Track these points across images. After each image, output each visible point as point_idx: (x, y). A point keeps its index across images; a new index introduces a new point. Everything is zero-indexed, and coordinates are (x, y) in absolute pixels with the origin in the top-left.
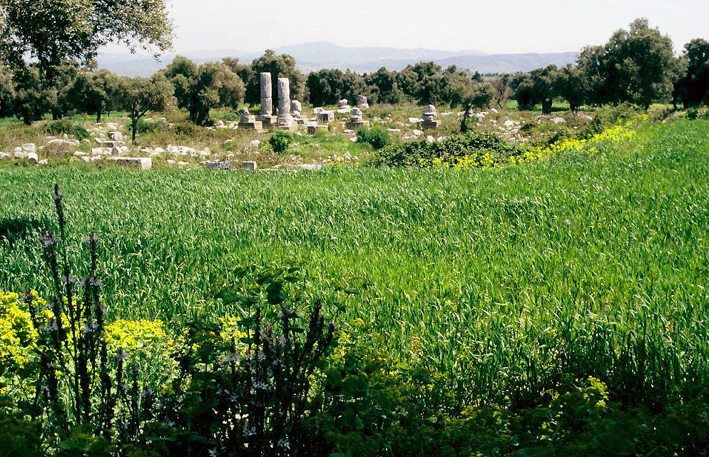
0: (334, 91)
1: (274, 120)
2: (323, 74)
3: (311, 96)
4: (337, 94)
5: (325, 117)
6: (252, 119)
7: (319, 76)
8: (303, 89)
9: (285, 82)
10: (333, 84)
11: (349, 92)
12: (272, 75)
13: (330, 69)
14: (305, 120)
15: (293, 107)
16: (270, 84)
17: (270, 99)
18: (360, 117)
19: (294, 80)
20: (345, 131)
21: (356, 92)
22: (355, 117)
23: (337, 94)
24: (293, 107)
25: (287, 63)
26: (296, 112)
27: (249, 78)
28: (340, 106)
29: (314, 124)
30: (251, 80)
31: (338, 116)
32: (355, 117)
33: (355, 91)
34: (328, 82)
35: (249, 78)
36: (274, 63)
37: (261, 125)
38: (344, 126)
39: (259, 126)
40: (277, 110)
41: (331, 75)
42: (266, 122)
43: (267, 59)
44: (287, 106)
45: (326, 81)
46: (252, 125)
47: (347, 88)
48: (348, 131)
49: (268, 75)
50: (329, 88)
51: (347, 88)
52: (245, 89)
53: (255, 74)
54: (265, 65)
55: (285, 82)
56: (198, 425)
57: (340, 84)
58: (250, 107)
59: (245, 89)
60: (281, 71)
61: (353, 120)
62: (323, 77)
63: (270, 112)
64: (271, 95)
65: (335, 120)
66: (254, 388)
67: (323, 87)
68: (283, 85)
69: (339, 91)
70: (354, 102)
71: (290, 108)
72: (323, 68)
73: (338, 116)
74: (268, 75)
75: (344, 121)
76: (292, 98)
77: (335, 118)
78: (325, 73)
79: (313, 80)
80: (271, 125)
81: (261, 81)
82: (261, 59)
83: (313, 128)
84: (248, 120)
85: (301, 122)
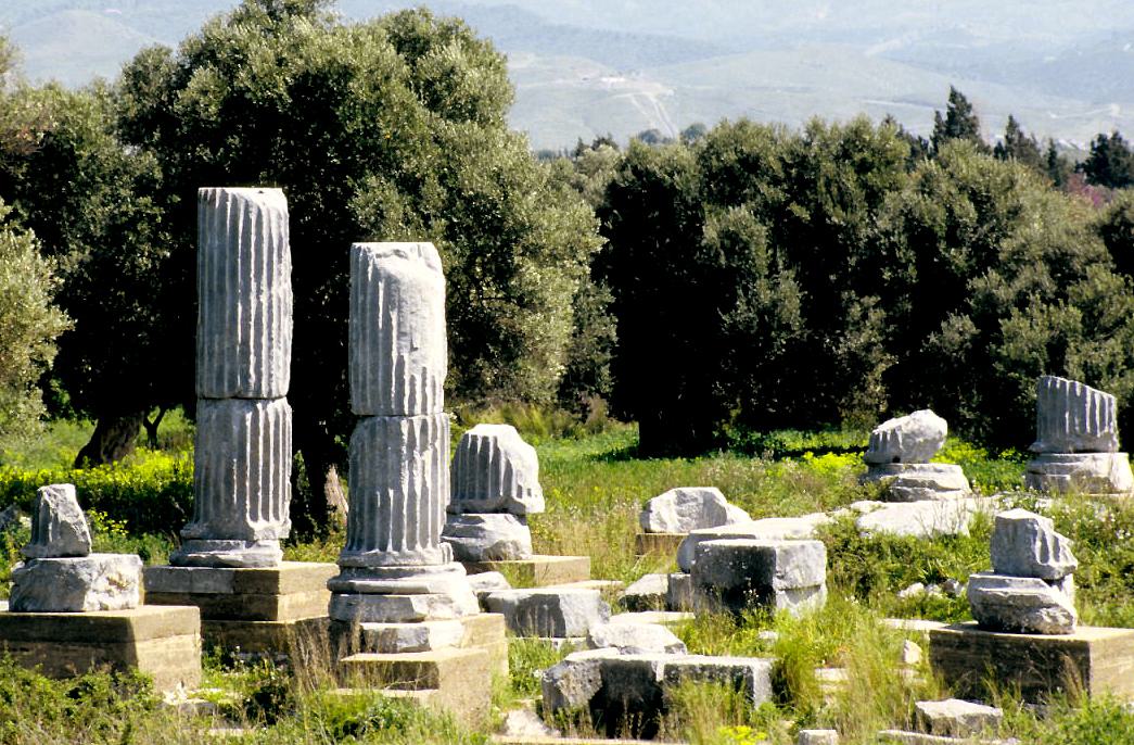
0: (824, 312)
1: (303, 590)
2: (732, 171)
3: (626, 357)
4: (854, 341)
5: (743, 583)
6: (112, 581)
7: (689, 183)
8: (560, 310)
9: (412, 272)
10: (812, 245)
11: (958, 328)
12: (295, 212)
13: (794, 125)
14: (579, 598)
15: (477, 483)
16: (282, 290)
17: (278, 412)
18: (1063, 597)
19: (484, 243)
20: (932, 709)
21: (1026, 332)
22: (1020, 587)
23: (854, 341)
24: (477, 483)
25: (437, 93)
26: (498, 528)
27: (96, 210)
28: (882, 472)
29: (652, 641)
30: (117, 231)
31: (862, 569)
32: (1020, 587)
33: (1016, 323)
34: (776, 239)
35: (96, 210)
36: (320, 91)
37: (192, 642)
38: (915, 654)
39: (170, 645)
40: (337, 491)
41: (800, 172)
42: (236, 616)
43: (261, 54)
44: (427, 477)
45: (761, 231)
46: (112, 639)
47: (942, 292)
48: (956, 709)
49: (269, 204)
50: (784, 292)
51: (942, 292)
52: (60, 321)
53: (143, 186)
54: (235, 105)
55: (412, 272)
56: (1052, 656)
57: (877, 255)
58: (93, 454)
59: (60, 321)
60: (382, 160)
61: (995, 617)
62: (736, 200)
63: (271, 527)
64: (282, 383)
65: (836, 607)
66: (988, 647)
67: (726, 278)
68: (393, 301)
69: (865, 327)
70: (1005, 424)
71: (444, 498)
72: (770, 546)
73: (862, 569)
74: (269, 204)
75: (922, 609)
76: (466, 387)
77: (837, 582)
78: (751, 164)
79: (646, 215)
80: (277, 647)
81: (209, 243)
82: (203, 54)
83: (640, 673)
84: (77, 586)
85: (536, 617)
